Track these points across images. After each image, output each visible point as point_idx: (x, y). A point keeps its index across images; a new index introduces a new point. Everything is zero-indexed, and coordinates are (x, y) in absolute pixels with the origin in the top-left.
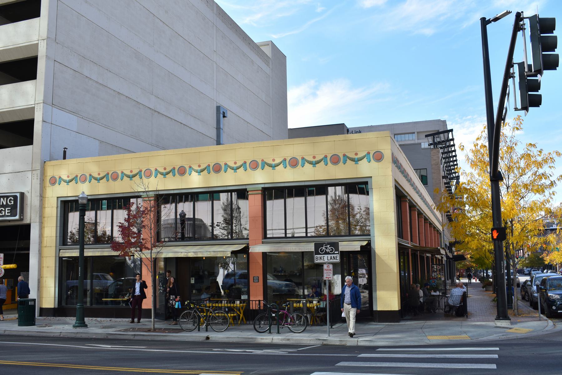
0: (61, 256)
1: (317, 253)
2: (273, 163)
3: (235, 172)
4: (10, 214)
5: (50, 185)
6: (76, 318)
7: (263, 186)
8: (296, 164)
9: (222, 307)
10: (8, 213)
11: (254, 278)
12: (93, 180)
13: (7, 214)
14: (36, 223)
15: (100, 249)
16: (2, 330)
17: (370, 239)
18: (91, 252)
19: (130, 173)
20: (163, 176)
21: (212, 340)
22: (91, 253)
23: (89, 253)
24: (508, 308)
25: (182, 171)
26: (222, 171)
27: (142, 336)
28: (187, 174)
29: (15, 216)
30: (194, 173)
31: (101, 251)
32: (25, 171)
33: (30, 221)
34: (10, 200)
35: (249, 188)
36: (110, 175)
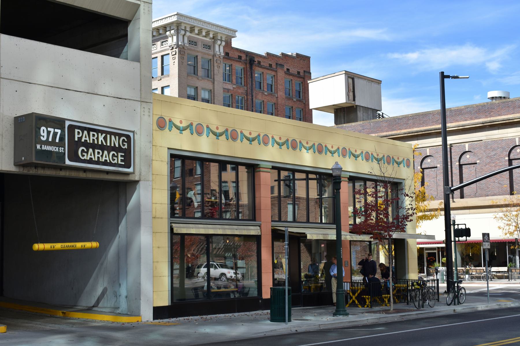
0: (176, 232)
1: (484, 242)
2: (218, 131)
3: (180, 133)
4: (123, 163)
5: (158, 129)
6: (269, 311)
7: (352, 174)
8: (200, 133)
9: (397, 286)
10: (122, 161)
11: (345, 263)
12: (245, 139)
13: (120, 162)
14: (148, 182)
15: (193, 225)
16: (317, 325)
17: (261, 224)
18: (254, 230)
19: (249, 135)
20: (249, 142)
21: (456, 312)
22: (212, 230)
23: (210, 230)
24: (290, 290)
25: (265, 141)
26: (298, 149)
27: (421, 314)
28: (298, 150)
29: (129, 167)
30: (303, 150)
31: (222, 229)
32: (130, 99)
33: (139, 177)
34: (123, 140)
35: (262, 164)
36: (261, 137)
